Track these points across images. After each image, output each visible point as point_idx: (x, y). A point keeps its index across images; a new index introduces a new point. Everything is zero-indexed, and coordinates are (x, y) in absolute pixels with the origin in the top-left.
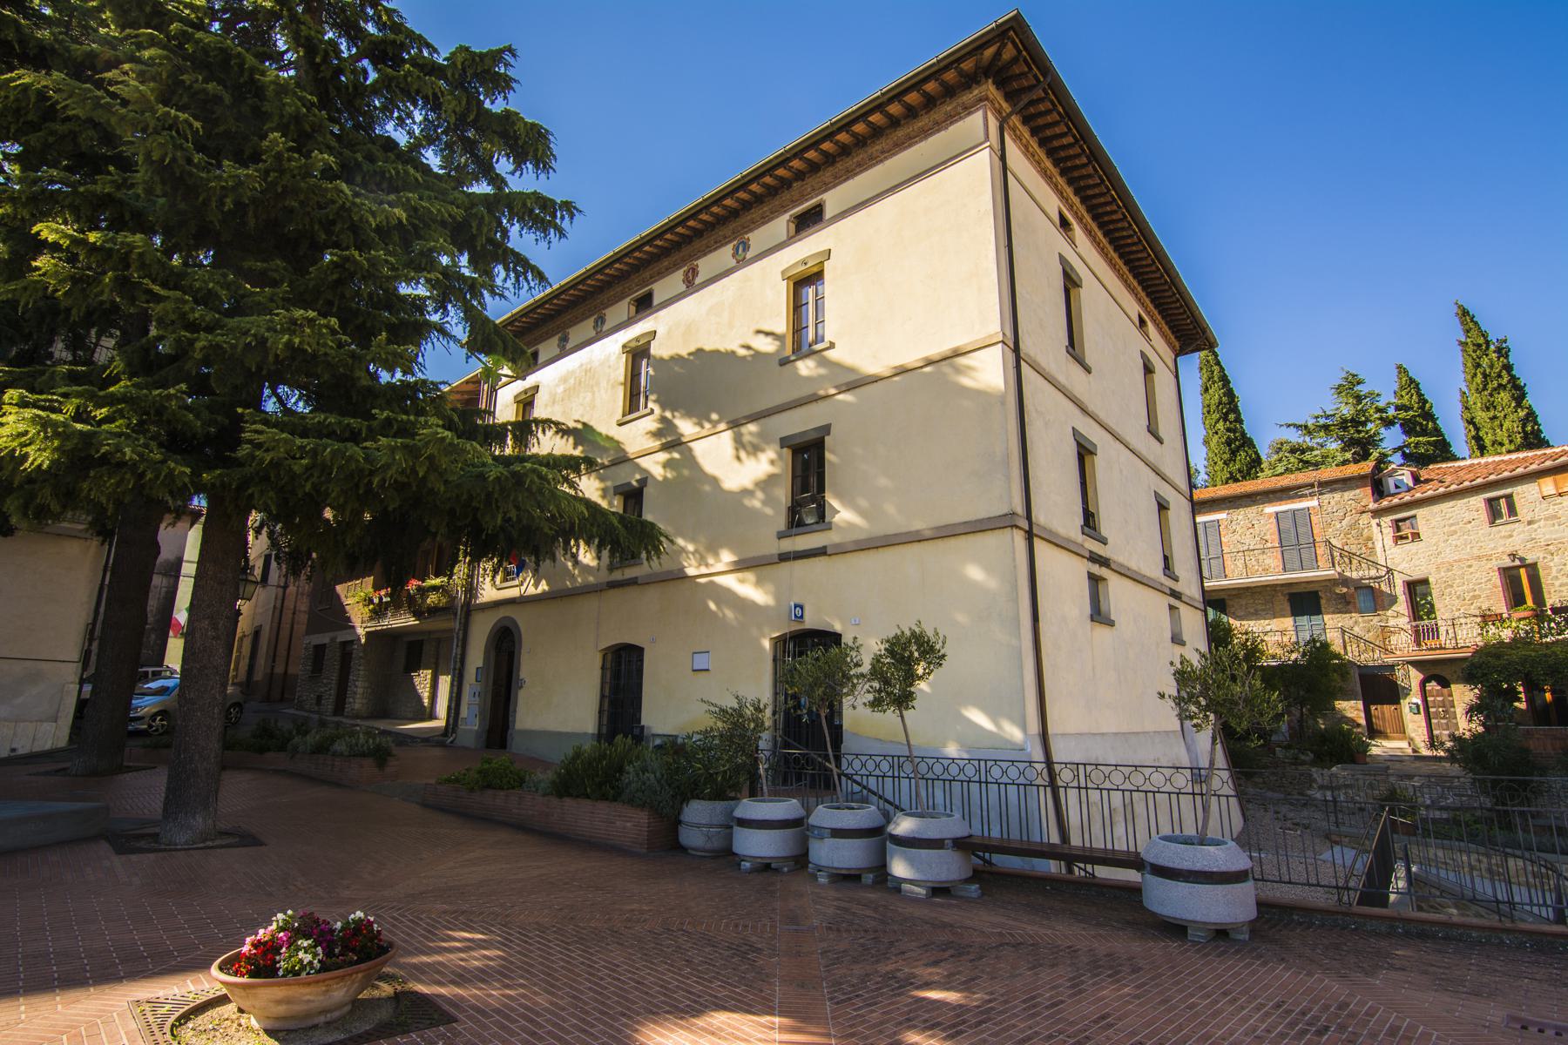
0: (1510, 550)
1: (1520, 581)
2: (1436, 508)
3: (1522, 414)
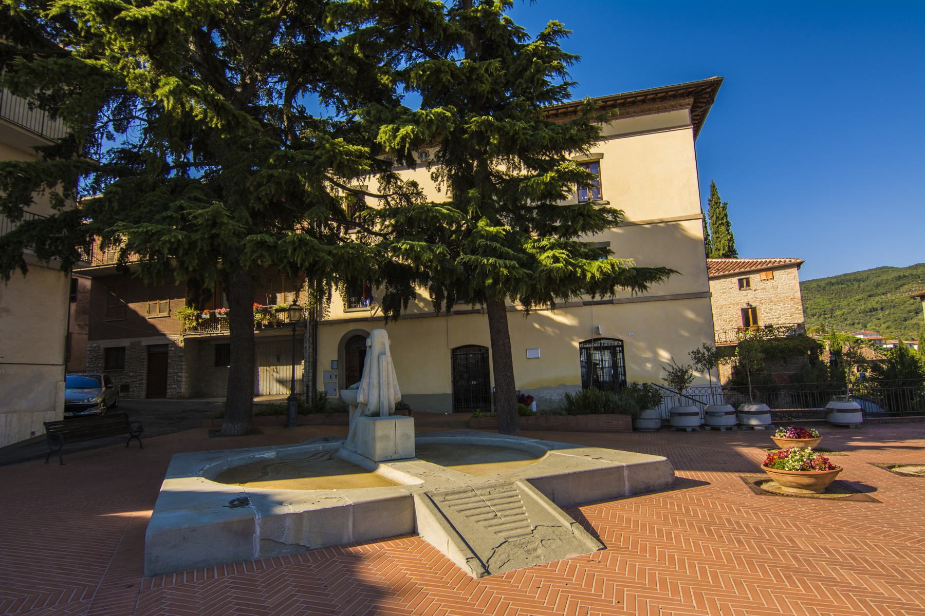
0: (746, 301)
1: (749, 315)
2: (718, 281)
3: (729, 237)
